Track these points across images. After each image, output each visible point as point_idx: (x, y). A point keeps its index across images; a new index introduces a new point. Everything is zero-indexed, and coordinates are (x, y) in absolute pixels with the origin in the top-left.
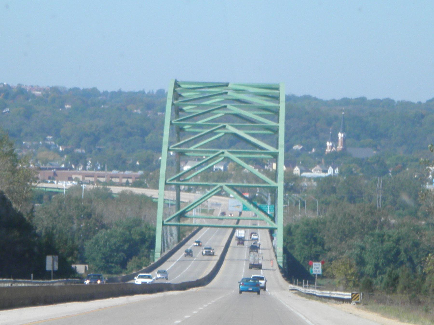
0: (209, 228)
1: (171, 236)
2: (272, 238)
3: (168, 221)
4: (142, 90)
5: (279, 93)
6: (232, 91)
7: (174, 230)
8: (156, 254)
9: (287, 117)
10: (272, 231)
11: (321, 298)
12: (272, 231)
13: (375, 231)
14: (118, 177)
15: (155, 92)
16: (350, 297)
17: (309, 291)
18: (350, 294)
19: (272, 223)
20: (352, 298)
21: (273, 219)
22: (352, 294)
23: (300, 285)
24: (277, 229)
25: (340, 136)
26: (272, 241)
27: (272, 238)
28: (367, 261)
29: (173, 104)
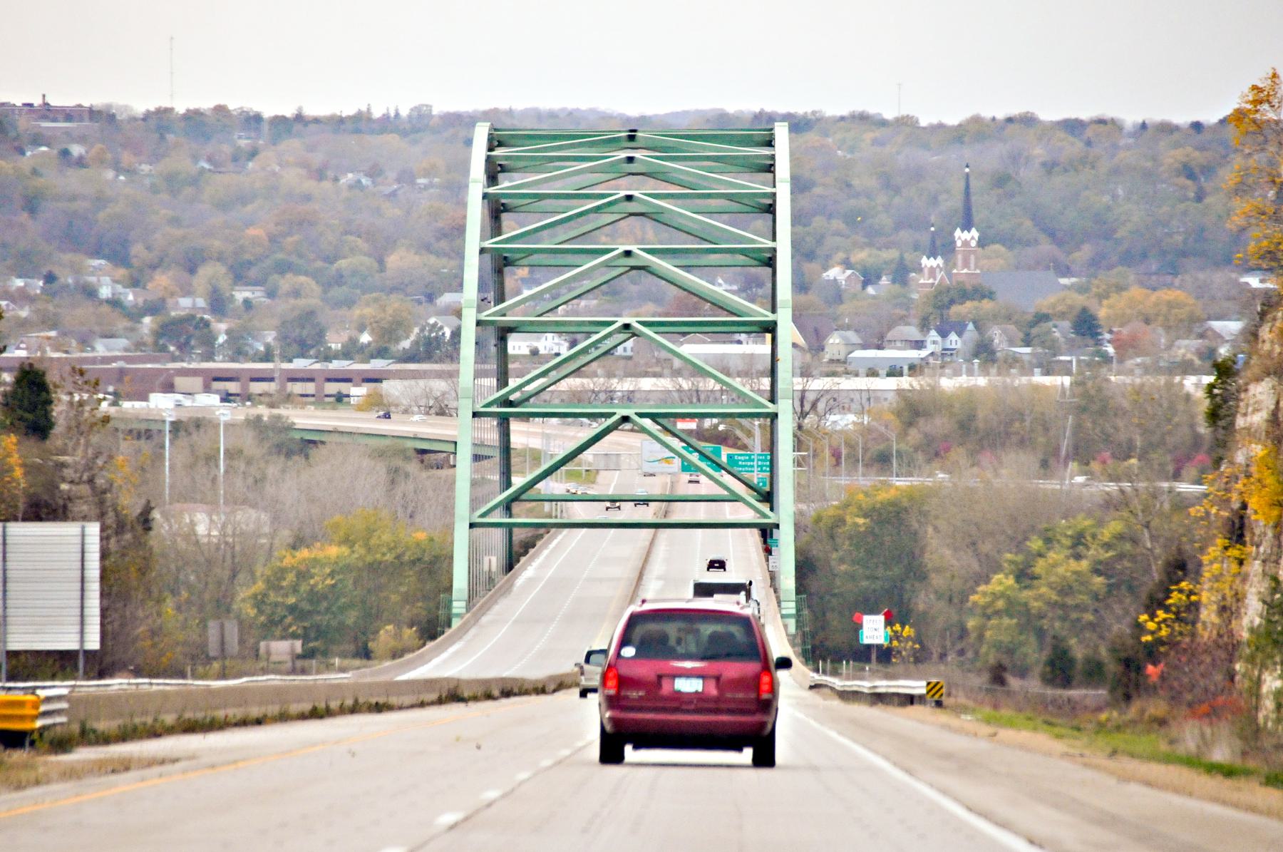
0: (585, 530)
1: (938, 687)
2: (768, 551)
3: (482, 516)
4: (364, 109)
5: (773, 157)
6: (769, 540)
7: (498, 536)
8: (455, 604)
9: (796, 219)
10: (767, 532)
11: (879, 698)
12: (767, 532)
13: (700, 690)
14: (311, 380)
15: (404, 113)
16: (924, 691)
17: (852, 686)
18: (924, 683)
19: (764, 508)
20: (928, 693)
21: (768, 497)
22: (929, 684)
23: (835, 673)
24: (777, 526)
25: (959, 238)
26: (767, 560)
27: (768, 551)
28: (907, 627)
29: (485, 196)
